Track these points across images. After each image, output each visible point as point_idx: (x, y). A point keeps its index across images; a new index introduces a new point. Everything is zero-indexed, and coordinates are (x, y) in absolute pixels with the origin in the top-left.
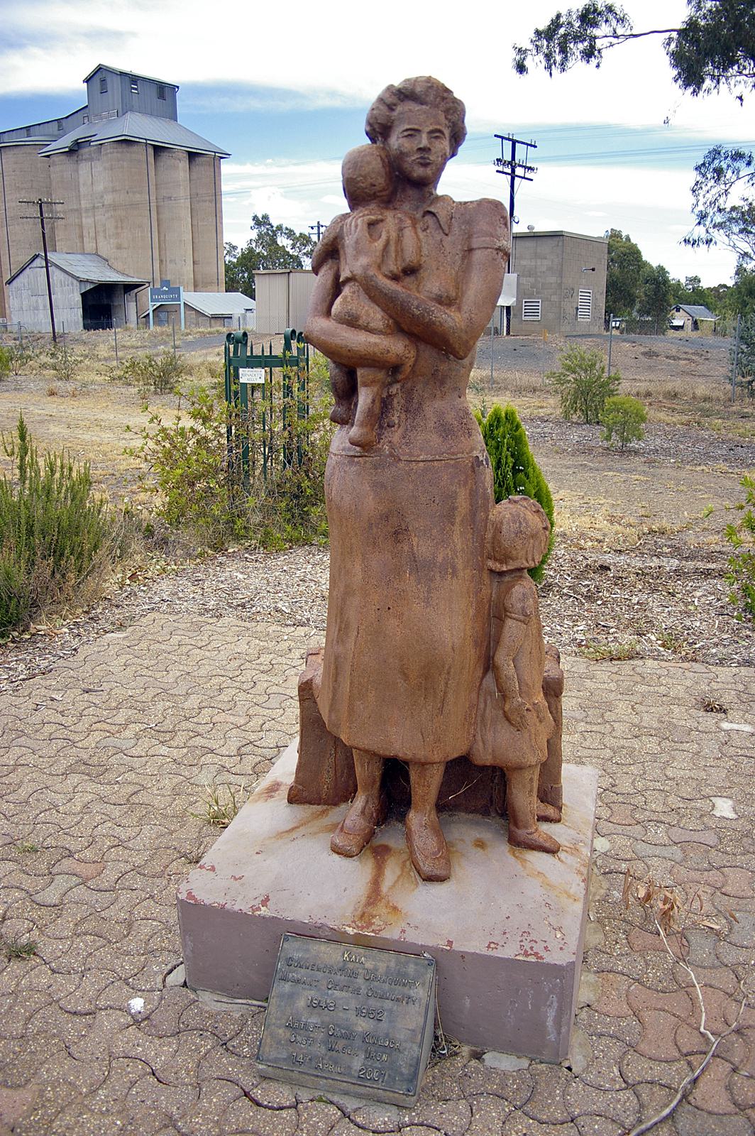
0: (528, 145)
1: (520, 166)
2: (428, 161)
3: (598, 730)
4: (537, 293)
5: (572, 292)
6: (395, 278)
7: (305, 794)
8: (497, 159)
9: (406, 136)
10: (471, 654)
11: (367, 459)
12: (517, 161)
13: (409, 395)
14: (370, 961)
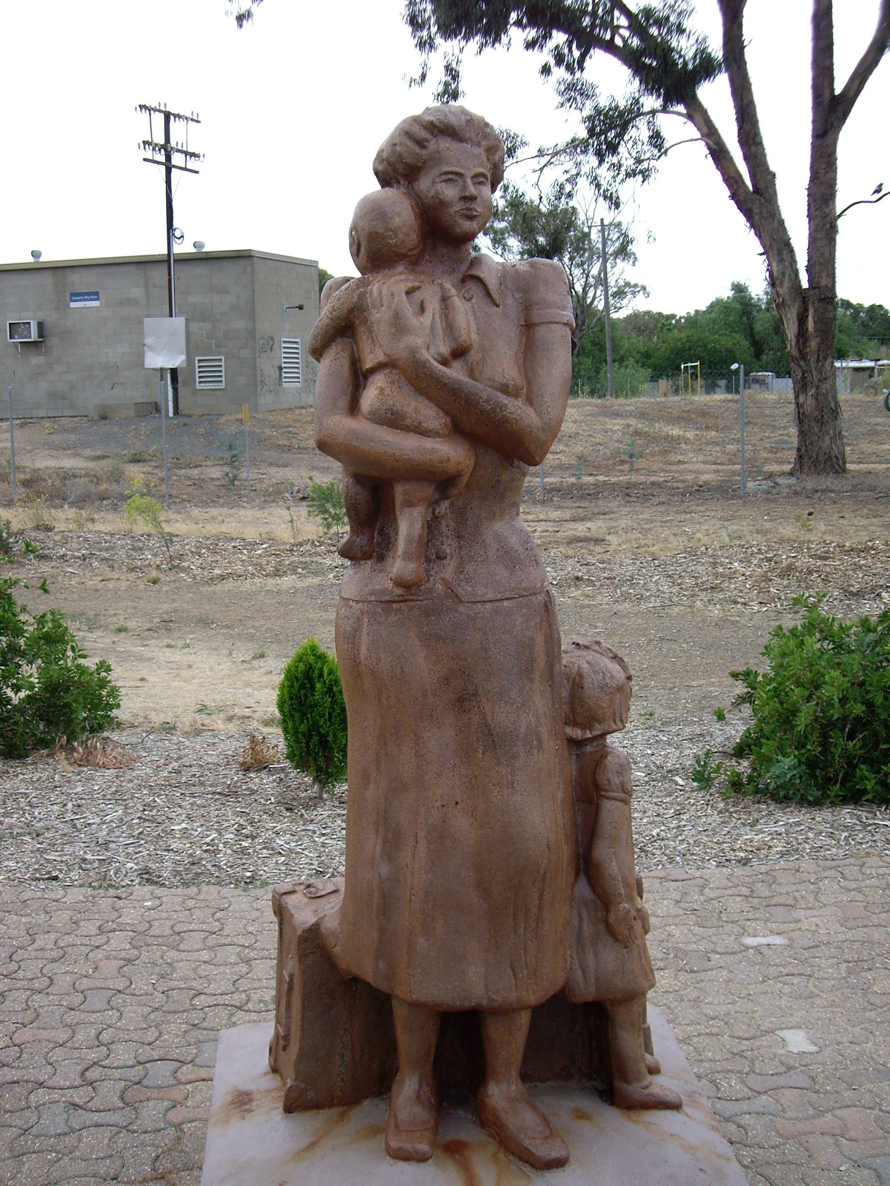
1: (178, 151)
2: (475, 213)
3: (91, 1114)
4: (218, 346)
5: (270, 344)
6: (445, 362)
7: (311, 1094)
8: (144, 142)
9: (444, 181)
10: (565, 852)
11: (413, 604)
12: (173, 144)
13: (461, 514)
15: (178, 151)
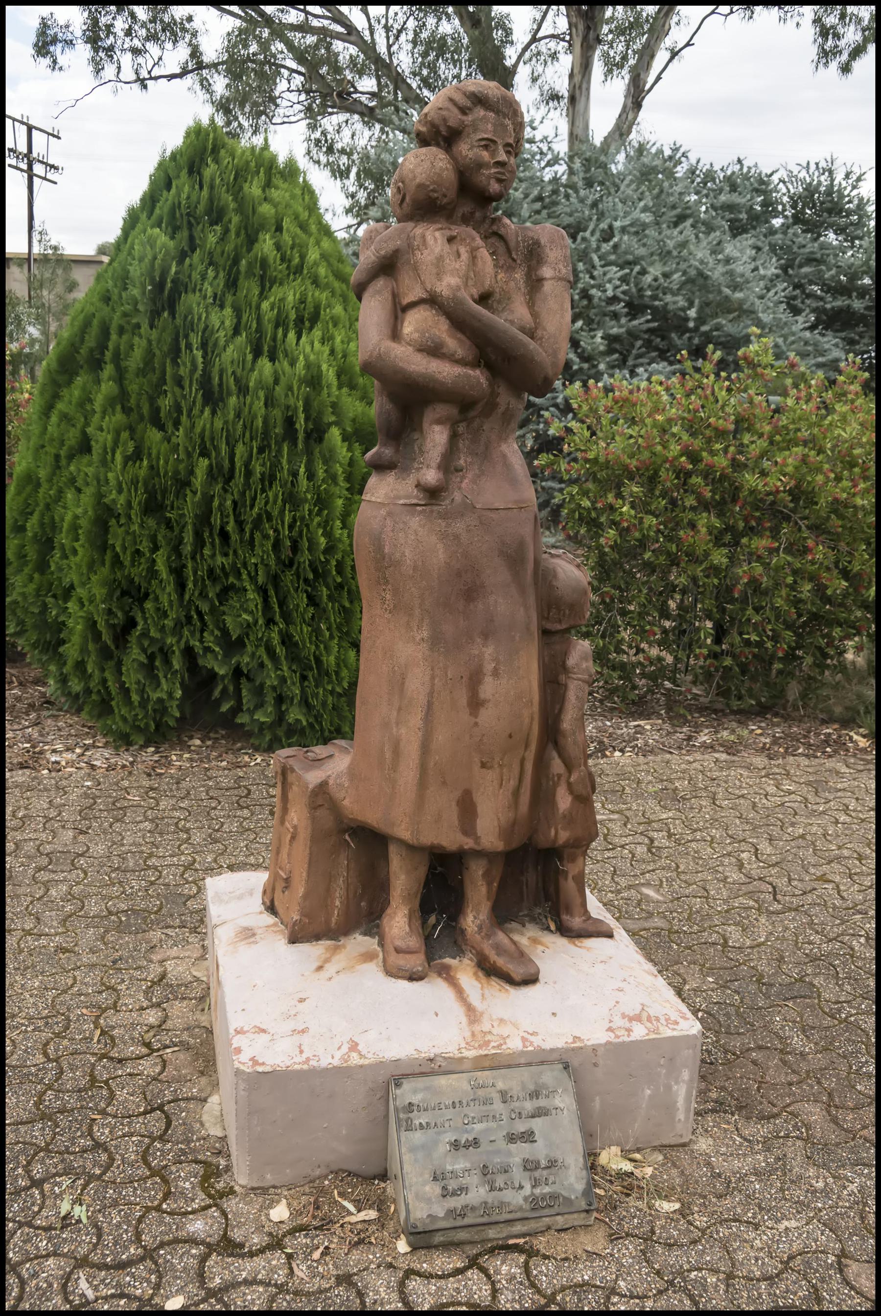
0: (49, 134)
12: (35, 155)
14: (503, 1081)
15: (39, 161)
